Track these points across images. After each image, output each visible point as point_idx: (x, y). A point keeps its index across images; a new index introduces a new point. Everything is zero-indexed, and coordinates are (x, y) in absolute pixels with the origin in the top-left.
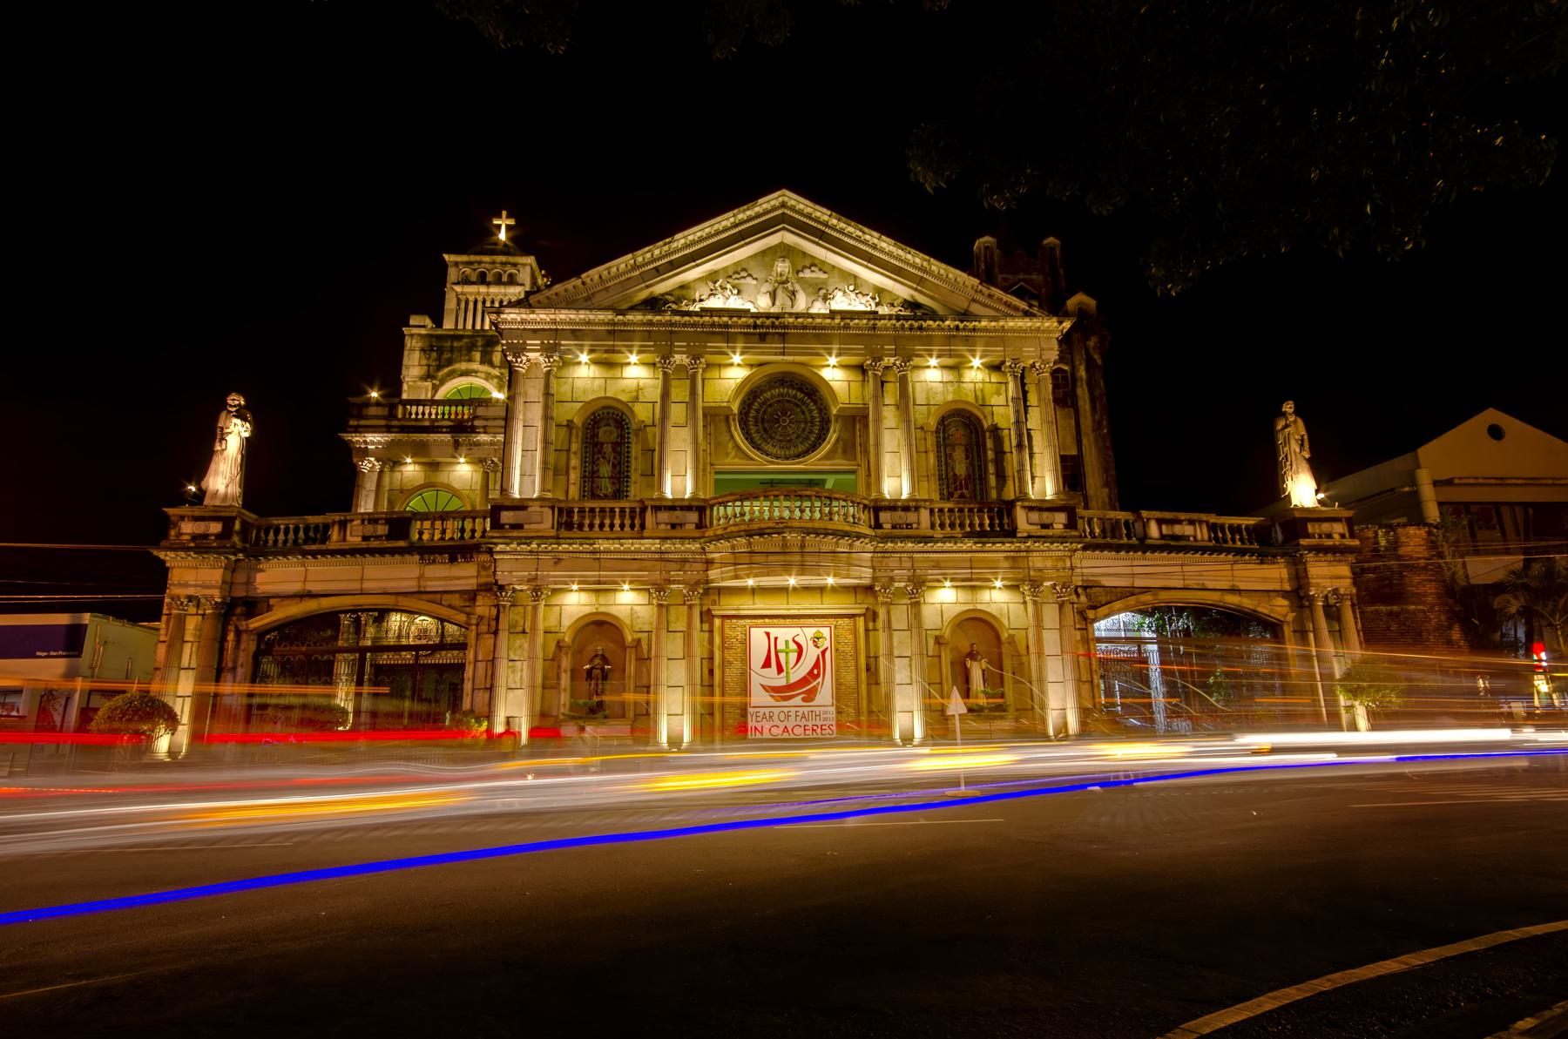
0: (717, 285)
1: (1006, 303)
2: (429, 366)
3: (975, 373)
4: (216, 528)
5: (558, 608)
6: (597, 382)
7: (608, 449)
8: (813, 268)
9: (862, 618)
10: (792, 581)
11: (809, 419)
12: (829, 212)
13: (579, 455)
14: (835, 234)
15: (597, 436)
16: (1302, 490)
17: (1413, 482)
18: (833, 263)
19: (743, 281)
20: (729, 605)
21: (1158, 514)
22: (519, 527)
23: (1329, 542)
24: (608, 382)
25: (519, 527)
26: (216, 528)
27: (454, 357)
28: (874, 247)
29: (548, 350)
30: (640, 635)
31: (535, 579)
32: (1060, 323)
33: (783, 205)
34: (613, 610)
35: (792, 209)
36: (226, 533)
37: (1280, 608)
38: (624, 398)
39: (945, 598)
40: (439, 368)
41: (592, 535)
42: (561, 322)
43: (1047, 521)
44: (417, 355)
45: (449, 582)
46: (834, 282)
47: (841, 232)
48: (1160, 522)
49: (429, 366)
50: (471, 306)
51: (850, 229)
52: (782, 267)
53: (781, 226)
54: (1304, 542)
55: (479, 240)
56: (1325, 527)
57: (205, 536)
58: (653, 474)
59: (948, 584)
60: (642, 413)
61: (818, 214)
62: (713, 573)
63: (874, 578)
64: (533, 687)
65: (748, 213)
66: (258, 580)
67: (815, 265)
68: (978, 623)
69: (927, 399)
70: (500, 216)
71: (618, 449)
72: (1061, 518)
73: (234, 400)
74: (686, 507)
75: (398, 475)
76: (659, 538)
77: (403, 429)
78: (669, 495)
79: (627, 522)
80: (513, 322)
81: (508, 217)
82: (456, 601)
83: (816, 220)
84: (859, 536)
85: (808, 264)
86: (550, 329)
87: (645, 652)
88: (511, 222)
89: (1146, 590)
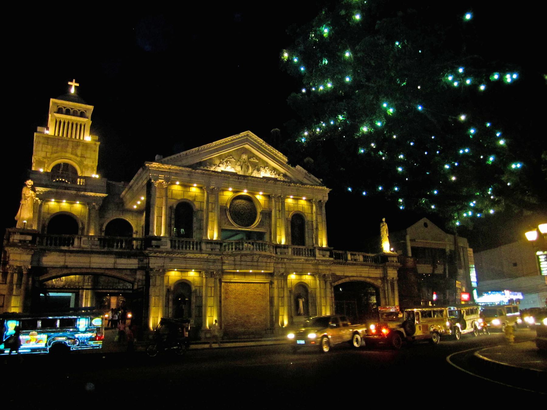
0: (224, 161)
1: (314, 180)
3: (303, 202)
4: (29, 238)
5: (168, 277)
9: (268, 284)
12: (263, 141)
13: (174, 220)
16: (386, 247)
19: (231, 160)
20: (227, 278)
25: (158, 247)
26: (29, 238)
28: (276, 155)
29: (167, 180)
30: (196, 288)
31: (163, 266)
33: (248, 135)
34: (187, 278)
35: (250, 137)
36: (33, 242)
37: (379, 283)
38: (190, 199)
41: (186, 251)
42: (172, 170)
43: (324, 254)
47: (266, 148)
48: (351, 254)
52: (245, 157)
55: (63, 94)
57: (25, 241)
58: (203, 229)
59: (294, 273)
60: (197, 205)
62: (224, 267)
64: (163, 306)
65: (237, 137)
66: (43, 261)
68: (302, 286)
69: (288, 209)
70: (72, 81)
74: (216, 243)
75: (47, 206)
76: (208, 254)
78: (209, 239)
80: (155, 167)
81: (76, 82)
82: (128, 272)
83: (258, 142)
85: (252, 156)
86: (167, 172)
87: (198, 294)
88: (78, 85)
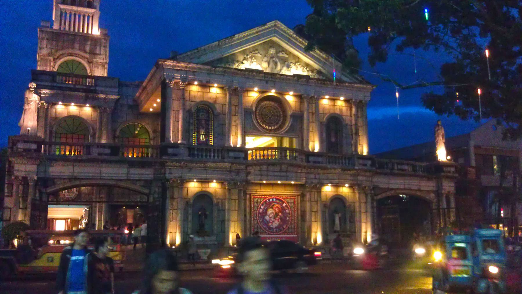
0: (248, 57)
2: (52, 49)
3: (341, 103)
6: (200, 94)
7: (203, 122)
8: (283, 52)
10: (279, 182)
11: (279, 115)
14: (294, 40)
15: (199, 117)
17: (467, 144)
18: (291, 51)
19: (256, 55)
21: (398, 161)
22: (175, 155)
23: (449, 174)
24: (204, 94)
25: (175, 155)
27: (65, 45)
32: (372, 87)
34: (208, 190)
39: (328, 190)
40: (57, 50)
43: (365, 163)
44: (45, 42)
45: (141, 176)
46: (291, 60)
49: (52, 49)
50: (68, 16)
51: (301, 40)
53: (273, 35)
54: (443, 174)
56: (449, 169)
61: (289, 32)
62: (249, 178)
63: (306, 182)
67: (284, 51)
69: (324, 112)
71: (207, 123)
72: (369, 162)
73: (32, 85)
77: (60, 88)
78: (232, 145)
79: (216, 155)
80: (170, 65)
84: (299, 166)
85: (281, 50)
89: (392, 189)
